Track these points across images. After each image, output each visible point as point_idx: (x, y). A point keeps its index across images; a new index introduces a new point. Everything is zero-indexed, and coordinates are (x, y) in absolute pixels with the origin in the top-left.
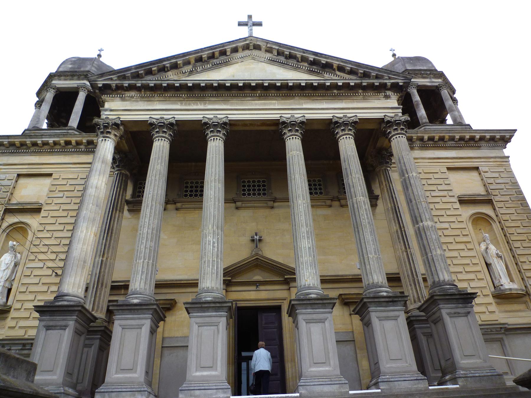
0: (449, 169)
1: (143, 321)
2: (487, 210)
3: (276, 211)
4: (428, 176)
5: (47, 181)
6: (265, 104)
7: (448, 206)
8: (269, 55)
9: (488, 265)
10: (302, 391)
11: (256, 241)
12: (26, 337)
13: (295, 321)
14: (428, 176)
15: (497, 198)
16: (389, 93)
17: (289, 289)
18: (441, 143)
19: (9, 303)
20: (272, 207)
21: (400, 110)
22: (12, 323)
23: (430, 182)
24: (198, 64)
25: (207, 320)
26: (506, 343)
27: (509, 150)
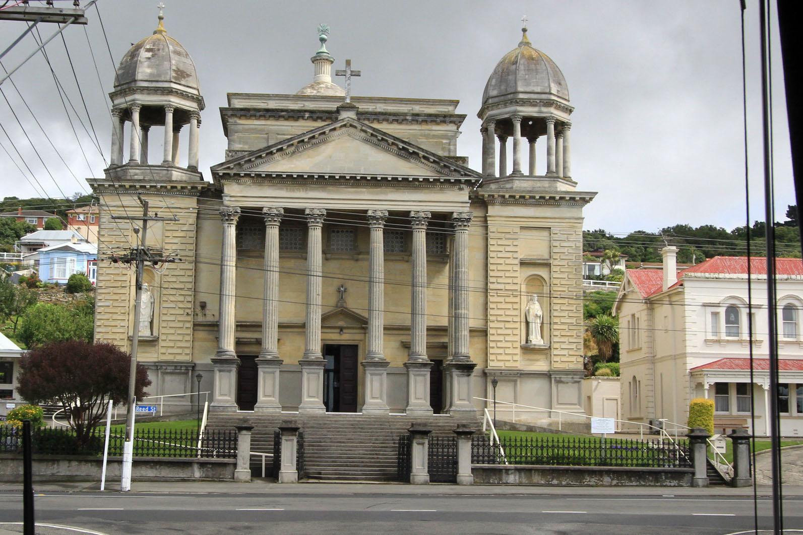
0: (522, 228)
1: (275, 370)
2: (543, 272)
3: (360, 263)
7: (509, 268)
8: (363, 134)
9: (527, 323)
10: (364, 412)
14: (500, 235)
15: (556, 263)
16: (462, 186)
17: (365, 333)
19: (155, 333)
20: (357, 260)
22: (163, 350)
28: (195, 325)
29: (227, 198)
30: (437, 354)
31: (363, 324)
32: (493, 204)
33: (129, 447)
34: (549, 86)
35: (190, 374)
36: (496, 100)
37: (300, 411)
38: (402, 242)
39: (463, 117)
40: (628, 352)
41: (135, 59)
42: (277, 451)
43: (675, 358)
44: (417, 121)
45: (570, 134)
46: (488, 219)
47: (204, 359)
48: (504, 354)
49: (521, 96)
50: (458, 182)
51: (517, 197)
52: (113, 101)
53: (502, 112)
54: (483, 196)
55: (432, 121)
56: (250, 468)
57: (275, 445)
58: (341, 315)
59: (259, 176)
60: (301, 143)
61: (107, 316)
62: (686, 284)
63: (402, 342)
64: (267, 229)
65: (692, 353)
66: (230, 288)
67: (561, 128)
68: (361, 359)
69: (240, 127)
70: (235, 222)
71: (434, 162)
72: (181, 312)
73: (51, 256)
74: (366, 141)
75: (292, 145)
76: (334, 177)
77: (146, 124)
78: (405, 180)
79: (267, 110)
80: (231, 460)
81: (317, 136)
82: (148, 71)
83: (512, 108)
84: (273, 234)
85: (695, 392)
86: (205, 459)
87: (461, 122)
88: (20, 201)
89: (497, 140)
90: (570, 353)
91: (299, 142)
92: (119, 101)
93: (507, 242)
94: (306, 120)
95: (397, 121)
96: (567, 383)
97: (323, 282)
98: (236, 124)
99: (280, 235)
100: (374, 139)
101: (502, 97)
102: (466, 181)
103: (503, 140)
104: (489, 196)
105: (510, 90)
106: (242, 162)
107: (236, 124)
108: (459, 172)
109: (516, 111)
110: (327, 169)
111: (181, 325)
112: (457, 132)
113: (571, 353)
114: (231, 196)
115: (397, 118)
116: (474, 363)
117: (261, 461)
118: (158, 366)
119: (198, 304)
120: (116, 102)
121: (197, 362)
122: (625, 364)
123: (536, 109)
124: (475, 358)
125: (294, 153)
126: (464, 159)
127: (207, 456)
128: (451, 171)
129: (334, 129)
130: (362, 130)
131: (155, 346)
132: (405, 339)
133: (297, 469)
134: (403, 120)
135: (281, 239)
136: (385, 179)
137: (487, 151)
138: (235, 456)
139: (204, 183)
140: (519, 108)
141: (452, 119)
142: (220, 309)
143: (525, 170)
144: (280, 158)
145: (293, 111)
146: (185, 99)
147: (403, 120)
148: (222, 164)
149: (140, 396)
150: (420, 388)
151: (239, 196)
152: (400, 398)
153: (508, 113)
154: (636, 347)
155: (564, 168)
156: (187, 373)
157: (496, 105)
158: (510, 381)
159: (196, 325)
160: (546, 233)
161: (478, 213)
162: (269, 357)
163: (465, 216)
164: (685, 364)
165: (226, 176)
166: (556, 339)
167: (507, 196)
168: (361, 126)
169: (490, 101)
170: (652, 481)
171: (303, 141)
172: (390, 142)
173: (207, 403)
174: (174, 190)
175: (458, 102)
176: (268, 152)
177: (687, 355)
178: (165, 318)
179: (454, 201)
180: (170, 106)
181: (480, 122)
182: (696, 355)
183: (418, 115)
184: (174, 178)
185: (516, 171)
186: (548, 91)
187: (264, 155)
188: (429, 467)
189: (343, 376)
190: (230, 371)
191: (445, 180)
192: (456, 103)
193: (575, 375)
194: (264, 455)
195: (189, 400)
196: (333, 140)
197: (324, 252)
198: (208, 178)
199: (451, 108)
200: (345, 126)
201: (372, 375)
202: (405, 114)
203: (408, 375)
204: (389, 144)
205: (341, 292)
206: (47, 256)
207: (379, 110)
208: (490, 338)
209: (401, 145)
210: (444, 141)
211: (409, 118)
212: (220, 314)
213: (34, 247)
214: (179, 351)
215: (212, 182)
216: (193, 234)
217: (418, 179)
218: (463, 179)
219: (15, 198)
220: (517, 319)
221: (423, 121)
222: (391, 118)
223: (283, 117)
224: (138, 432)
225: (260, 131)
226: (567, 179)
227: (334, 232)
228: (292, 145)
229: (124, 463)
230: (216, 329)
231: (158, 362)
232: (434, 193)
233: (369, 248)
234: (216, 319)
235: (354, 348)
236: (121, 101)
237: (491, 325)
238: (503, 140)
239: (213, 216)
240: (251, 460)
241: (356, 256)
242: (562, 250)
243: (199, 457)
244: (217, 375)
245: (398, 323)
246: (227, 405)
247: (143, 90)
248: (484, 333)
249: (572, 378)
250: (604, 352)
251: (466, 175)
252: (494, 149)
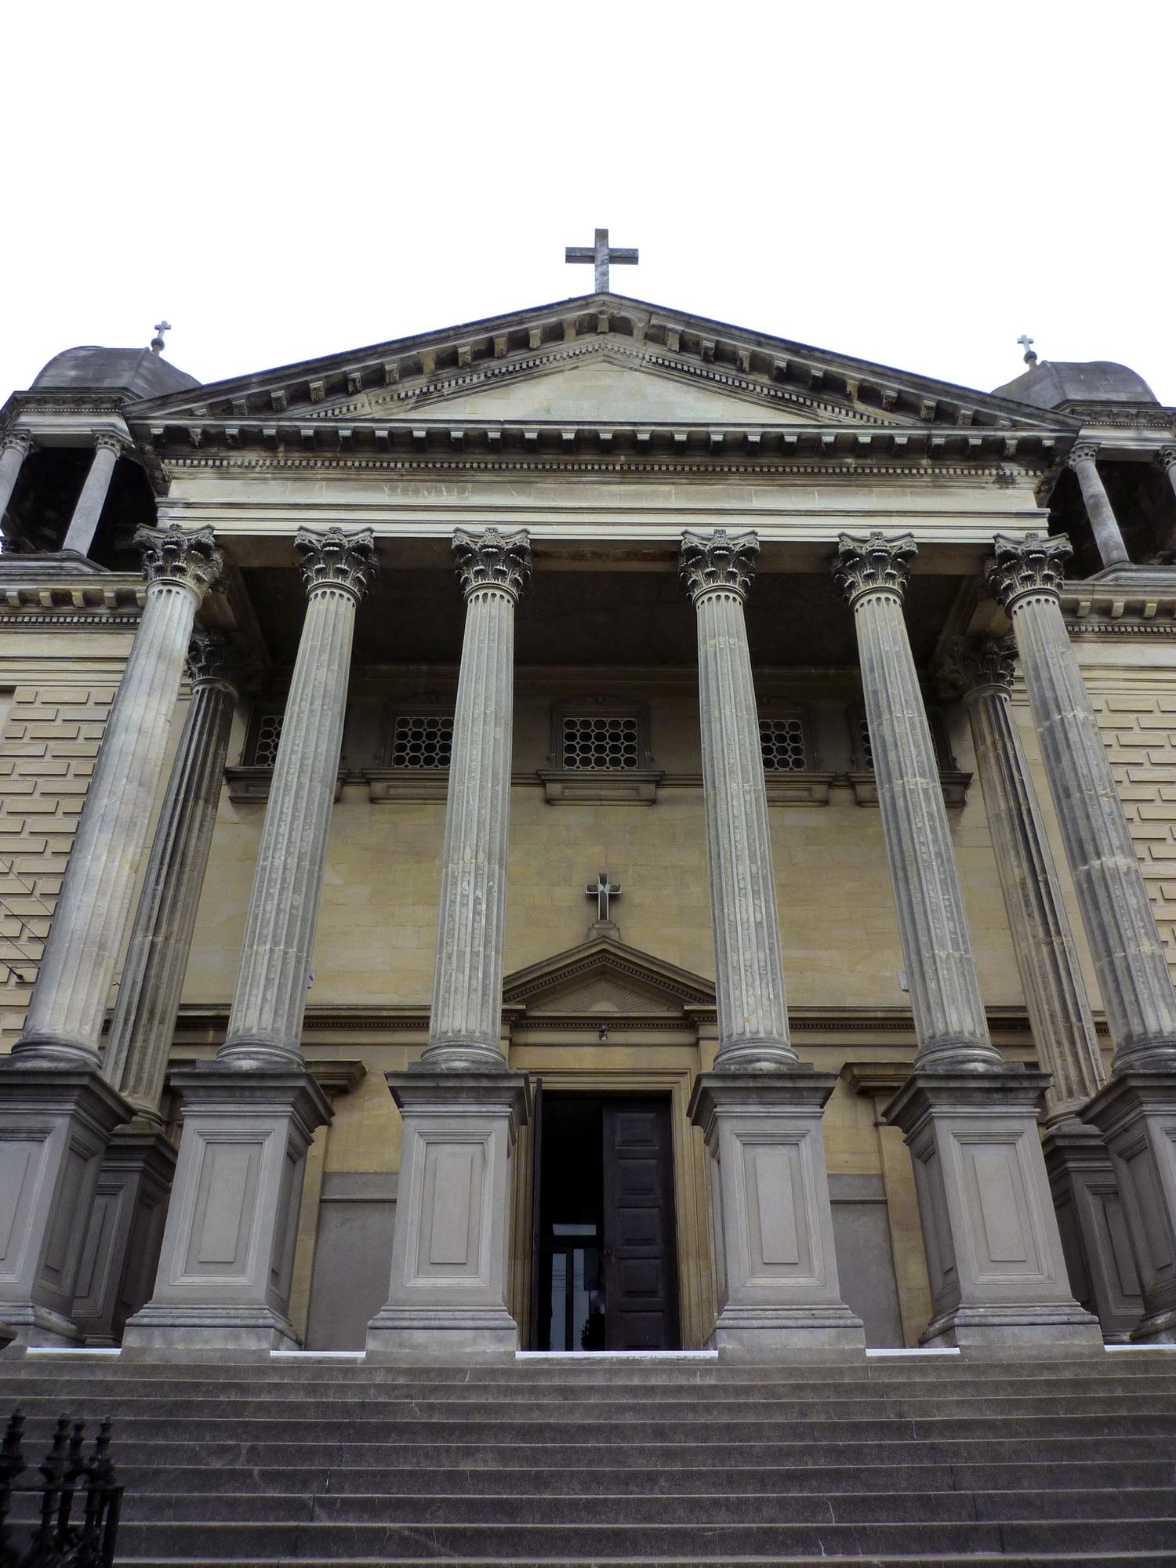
3: (662, 813)
8: (653, 350)
10: (728, 1343)
20: (652, 802)
25: (454, 1125)
37: (372, 1344)
168: (645, 316)
190: (38, 1135)
239: (200, 718)
241: (648, 790)
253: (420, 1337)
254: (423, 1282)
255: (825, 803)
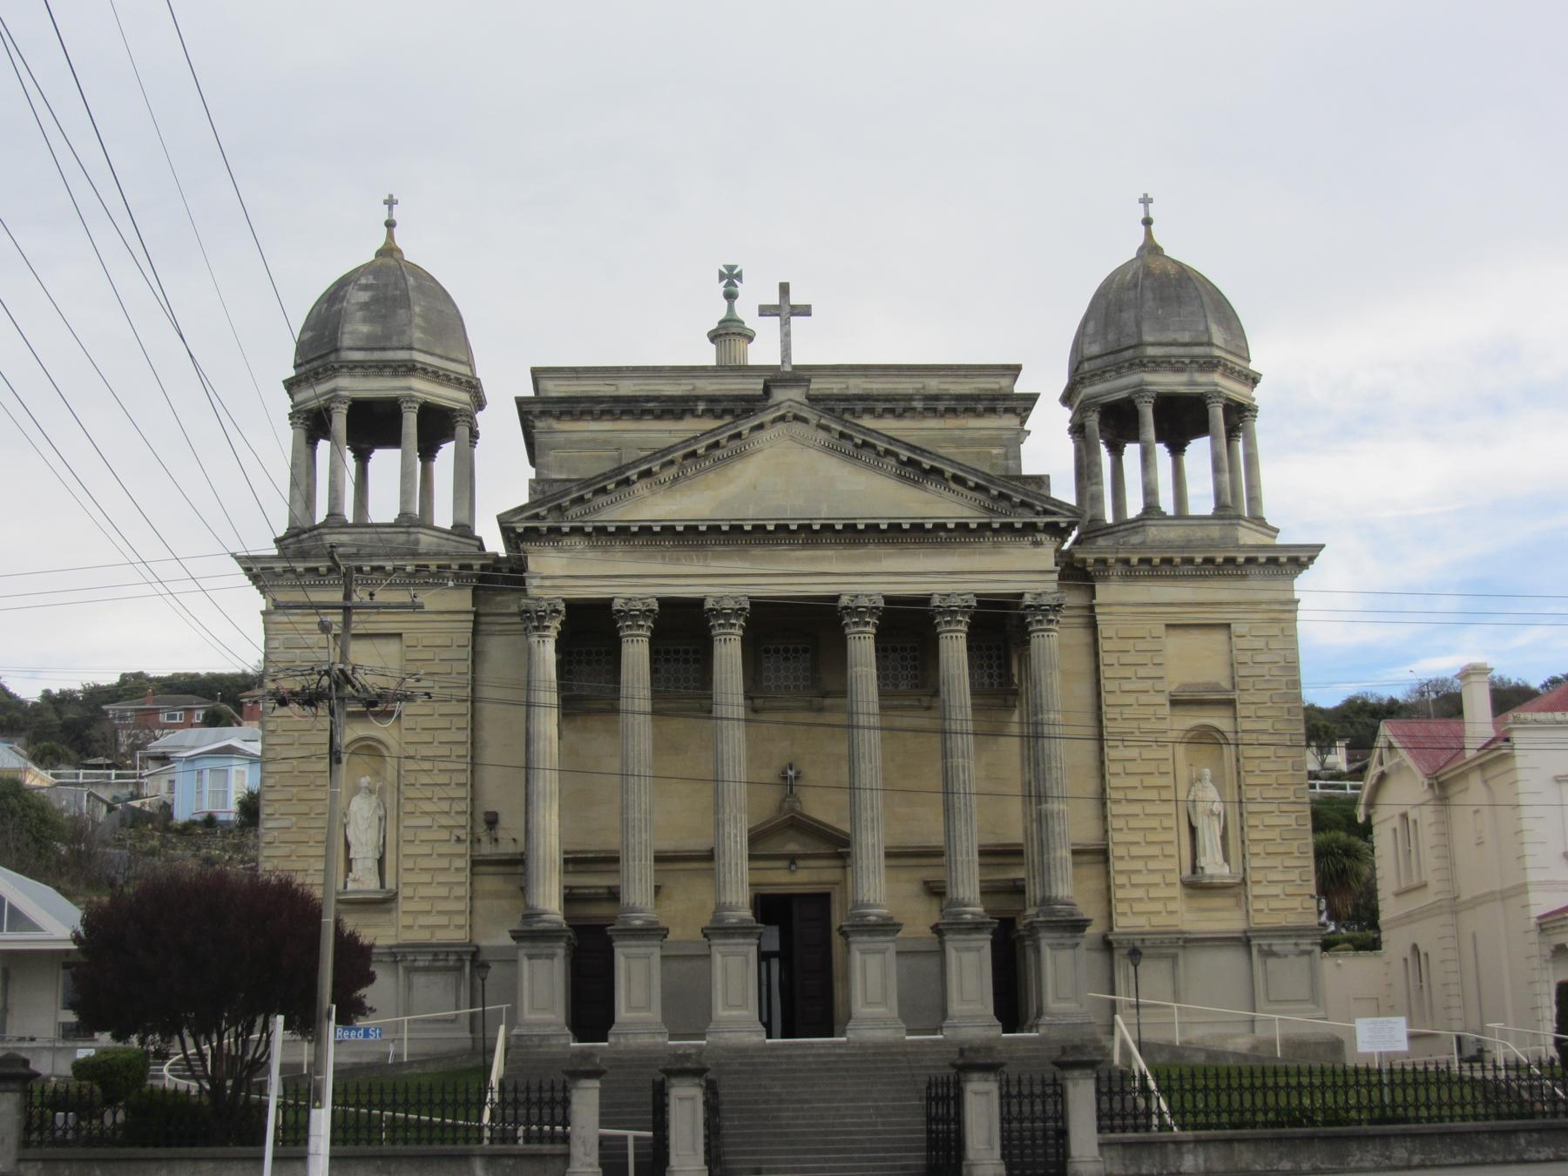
0: (1168, 626)
1: (651, 950)
2: (1218, 720)
4: (1122, 645)
5: (392, 647)
6: (813, 560)
8: (822, 435)
9: (1193, 830)
10: (850, 1035)
11: (789, 781)
12: (434, 941)
13: (848, 945)
14: (1122, 645)
15: (1246, 697)
16: (1039, 537)
17: (844, 867)
18: (1166, 569)
19: (390, 883)
21: (1055, 576)
22: (407, 921)
23: (1126, 659)
24: (688, 462)
25: (733, 949)
26: (1181, 963)
27: (1304, 584)
28: (475, 863)
29: (535, 582)
30: (1005, 904)
31: (838, 846)
32: (1106, 579)
33: (321, 1121)
34: (1207, 329)
35: (467, 969)
36: (1099, 362)
38: (915, 668)
39: (1031, 399)
40: (1398, 895)
41: (337, 307)
42: (660, 1124)
43: (1504, 896)
44: (935, 410)
45: (1261, 426)
46: (1097, 610)
47: (497, 938)
48: (1148, 901)
49: (1151, 351)
50: (1030, 528)
51: (1157, 561)
52: (292, 396)
53: (1113, 388)
54: (1084, 561)
55: (967, 410)
56: (601, 1165)
57: (655, 1113)
58: (788, 829)
59: (601, 531)
60: (691, 460)
61: (284, 850)
62: (1516, 736)
63: (926, 883)
64: (624, 646)
65: (1540, 883)
66: (548, 783)
67: (1239, 415)
68: (837, 919)
69: (561, 438)
70: (553, 633)
71: (978, 488)
72: (445, 835)
73: (199, 765)
74: (830, 449)
75: (672, 462)
76: (764, 527)
77: (364, 446)
78: (917, 528)
79: (617, 399)
80: (559, 1148)
81: (723, 442)
82: (364, 329)
83: (1133, 378)
84: (636, 652)
85: (1550, 965)
86: (497, 1147)
87: (1029, 410)
88: (151, 680)
89: (1104, 450)
90: (1287, 890)
91: (686, 457)
92: (304, 394)
93: (1151, 640)
94: (699, 417)
95: (892, 411)
96: (1286, 956)
97: (749, 794)
98: (551, 431)
99: (654, 660)
100: (848, 445)
101: (1111, 357)
102: (1048, 525)
103: (1116, 451)
104: (1096, 560)
105: (1126, 342)
106: (565, 502)
107: (551, 431)
108: (1030, 506)
109: (1141, 384)
110: (749, 513)
111: (444, 863)
112: (1021, 434)
113: (1290, 890)
114: (543, 578)
115: (897, 406)
116: (1086, 916)
117: (626, 1147)
118: (398, 955)
119: (480, 818)
120: (299, 397)
121: (483, 943)
122: (1393, 920)
123: (1183, 378)
124: (1088, 908)
125: (676, 479)
126: (1041, 481)
127: (503, 1141)
128: (1014, 506)
129: (761, 427)
130: (821, 427)
131: (389, 911)
132: (930, 874)
133: (706, 1162)
134: (905, 410)
135: (654, 671)
136: (873, 528)
137: (1085, 472)
138: (566, 1139)
139: (486, 556)
140: (1149, 377)
141: (1008, 404)
142: (527, 822)
143: (1167, 503)
144: (646, 492)
145: (671, 399)
146: (441, 384)
147: (905, 410)
148: (521, 509)
149: (350, 1010)
150: (970, 972)
151: (560, 573)
152: (925, 1004)
153: (1127, 388)
154: (1415, 882)
155: (1250, 499)
156: (460, 969)
157: (1100, 374)
158: (1161, 957)
159: (477, 864)
160: (1219, 637)
161: (1074, 599)
162: (638, 923)
163: (1047, 600)
164: (1526, 906)
165: (532, 534)
166: (1256, 862)
167: (1134, 560)
169: (1086, 366)
170: (1497, 1153)
171: (694, 454)
172: (881, 449)
173: (502, 1028)
174: (426, 576)
175: (1018, 368)
176: (621, 480)
177: (1530, 888)
178: (409, 849)
179: (1024, 569)
180: (411, 399)
181: (1067, 414)
182: (1546, 885)
183: (937, 398)
184: (422, 548)
185: (1151, 508)
186: (1205, 339)
187: (611, 487)
188: (1003, 1147)
189: (801, 949)
191: (1003, 525)
192: (1015, 370)
193: (1300, 936)
194: (631, 1134)
195: (467, 1027)
196: (761, 450)
197: (748, 696)
198: (495, 544)
199: (1004, 382)
200: (782, 418)
201: (863, 952)
202: (909, 398)
203: (942, 953)
204: (878, 454)
205: (789, 781)
206: (188, 767)
207: (853, 391)
208: (1116, 865)
209: (905, 455)
210: (995, 451)
211: (918, 405)
212: (527, 831)
213: (163, 759)
214: (443, 920)
215: (502, 552)
216: (465, 667)
217: (944, 525)
218: (1041, 521)
219: (139, 676)
220: (1171, 823)
221: (948, 410)
222: (880, 406)
223: (650, 412)
224: (345, 1091)
225: (605, 443)
226: (1258, 520)
227: (767, 651)
228: (672, 462)
229: (311, 1159)
230: (520, 869)
231: (398, 946)
232: (982, 554)
233: (845, 684)
234: (520, 848)
235: (822, 901)
236: (312, 395)
237: (1115, 837)
238: (1116, 451)
240: (601, 1144)
241: (817, 701)
242: (1257, 671)
243: (486, 1142)
244: (525, 964)
245: (915, 840)
246: (549, 1031)
247: (353, 367)
248: (1101, 854)
249: (1296, 944)
250: (1348, 900)
251: (1046, 512)
252: (1099, 465)
253: (727, 1035)
254: (725, 1013)
255: (928, 708)
